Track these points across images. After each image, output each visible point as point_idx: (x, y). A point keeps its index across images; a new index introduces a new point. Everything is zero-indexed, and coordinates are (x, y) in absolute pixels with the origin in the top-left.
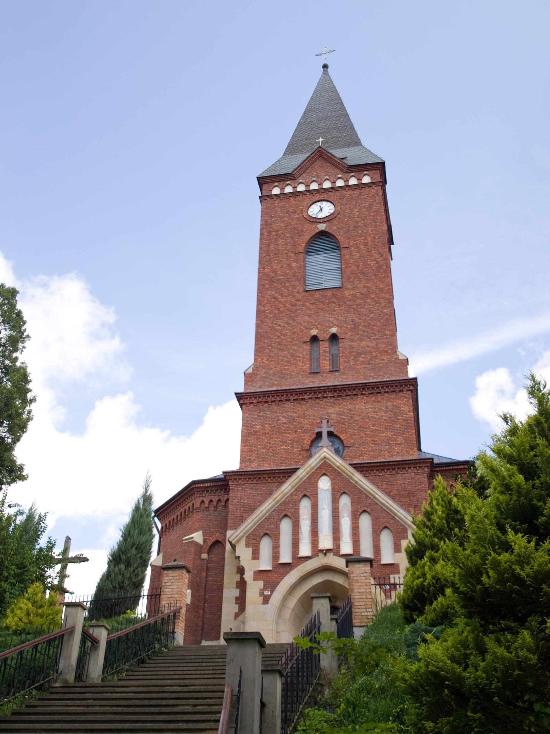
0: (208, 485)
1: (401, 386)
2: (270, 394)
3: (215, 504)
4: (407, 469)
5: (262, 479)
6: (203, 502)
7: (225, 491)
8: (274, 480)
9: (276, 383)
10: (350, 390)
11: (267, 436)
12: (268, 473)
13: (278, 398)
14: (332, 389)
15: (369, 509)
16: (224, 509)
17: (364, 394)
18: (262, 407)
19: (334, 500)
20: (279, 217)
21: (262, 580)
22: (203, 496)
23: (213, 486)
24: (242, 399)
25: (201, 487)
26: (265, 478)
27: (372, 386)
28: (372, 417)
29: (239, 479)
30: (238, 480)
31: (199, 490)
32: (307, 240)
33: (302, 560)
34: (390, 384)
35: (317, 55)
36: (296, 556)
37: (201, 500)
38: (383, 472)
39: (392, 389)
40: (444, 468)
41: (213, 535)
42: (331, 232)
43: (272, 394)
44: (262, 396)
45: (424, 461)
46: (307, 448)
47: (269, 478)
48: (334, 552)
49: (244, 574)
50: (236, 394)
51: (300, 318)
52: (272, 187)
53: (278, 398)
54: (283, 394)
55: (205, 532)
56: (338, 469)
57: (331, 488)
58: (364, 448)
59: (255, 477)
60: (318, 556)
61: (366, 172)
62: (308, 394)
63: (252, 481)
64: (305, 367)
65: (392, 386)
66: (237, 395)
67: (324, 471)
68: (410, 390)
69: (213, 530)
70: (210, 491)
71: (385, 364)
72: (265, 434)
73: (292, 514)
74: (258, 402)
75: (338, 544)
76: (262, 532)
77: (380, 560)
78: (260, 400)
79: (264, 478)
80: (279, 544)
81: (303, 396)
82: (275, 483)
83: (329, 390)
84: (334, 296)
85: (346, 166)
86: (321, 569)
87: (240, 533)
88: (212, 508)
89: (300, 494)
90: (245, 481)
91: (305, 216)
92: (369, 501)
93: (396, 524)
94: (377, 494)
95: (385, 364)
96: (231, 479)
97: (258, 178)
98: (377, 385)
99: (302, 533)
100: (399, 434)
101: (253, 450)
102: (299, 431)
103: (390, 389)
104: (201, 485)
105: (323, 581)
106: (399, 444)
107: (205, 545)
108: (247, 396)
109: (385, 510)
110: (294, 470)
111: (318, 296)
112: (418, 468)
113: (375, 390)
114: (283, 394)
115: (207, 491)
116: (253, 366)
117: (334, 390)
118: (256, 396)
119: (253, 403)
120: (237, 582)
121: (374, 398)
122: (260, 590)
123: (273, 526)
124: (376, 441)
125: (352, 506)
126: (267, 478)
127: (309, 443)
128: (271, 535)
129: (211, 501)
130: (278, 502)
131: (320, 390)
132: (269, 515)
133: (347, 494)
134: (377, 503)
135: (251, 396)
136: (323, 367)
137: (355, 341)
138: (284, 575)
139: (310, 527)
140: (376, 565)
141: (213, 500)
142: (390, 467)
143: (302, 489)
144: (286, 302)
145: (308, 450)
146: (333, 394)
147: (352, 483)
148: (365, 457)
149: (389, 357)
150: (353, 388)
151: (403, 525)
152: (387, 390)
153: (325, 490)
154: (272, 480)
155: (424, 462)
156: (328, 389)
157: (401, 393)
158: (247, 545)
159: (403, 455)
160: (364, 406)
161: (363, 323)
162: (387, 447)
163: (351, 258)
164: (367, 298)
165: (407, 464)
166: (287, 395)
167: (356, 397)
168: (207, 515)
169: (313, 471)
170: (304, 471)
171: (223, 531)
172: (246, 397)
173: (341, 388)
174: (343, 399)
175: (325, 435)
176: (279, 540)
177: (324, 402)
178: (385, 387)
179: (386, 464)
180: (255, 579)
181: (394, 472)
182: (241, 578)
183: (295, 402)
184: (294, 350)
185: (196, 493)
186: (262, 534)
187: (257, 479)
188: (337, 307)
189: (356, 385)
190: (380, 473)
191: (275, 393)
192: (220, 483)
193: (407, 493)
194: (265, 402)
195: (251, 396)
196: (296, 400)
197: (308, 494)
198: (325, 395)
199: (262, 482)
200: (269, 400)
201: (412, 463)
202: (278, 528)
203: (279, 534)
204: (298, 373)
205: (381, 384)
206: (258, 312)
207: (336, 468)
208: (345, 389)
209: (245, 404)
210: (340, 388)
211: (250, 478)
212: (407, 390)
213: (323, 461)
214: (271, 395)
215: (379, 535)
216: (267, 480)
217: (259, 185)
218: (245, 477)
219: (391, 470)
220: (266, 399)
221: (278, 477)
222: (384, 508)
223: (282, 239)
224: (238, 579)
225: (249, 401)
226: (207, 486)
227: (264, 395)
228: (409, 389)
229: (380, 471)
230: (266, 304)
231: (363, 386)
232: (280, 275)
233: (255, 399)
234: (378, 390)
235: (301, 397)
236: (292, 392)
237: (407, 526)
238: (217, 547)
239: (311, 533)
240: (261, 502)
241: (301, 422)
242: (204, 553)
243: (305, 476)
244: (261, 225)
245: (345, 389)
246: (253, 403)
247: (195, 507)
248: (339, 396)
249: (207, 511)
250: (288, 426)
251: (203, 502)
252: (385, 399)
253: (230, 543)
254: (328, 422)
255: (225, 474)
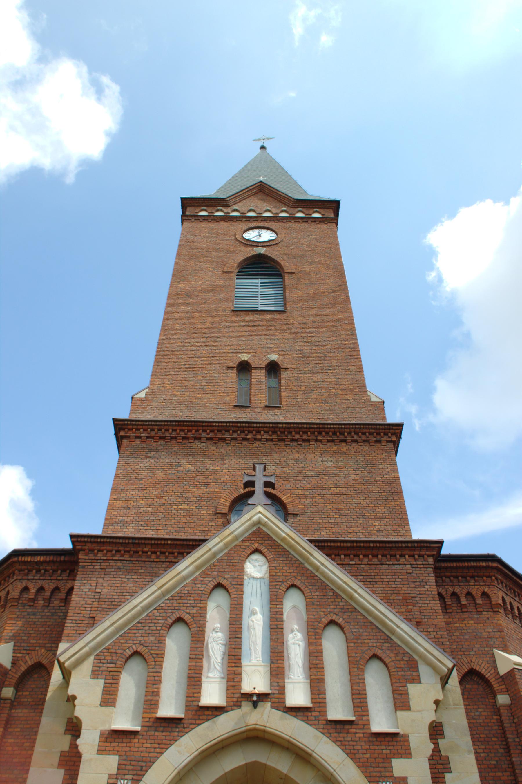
0: (42, 560)
1: (379, 434)
2: (170, 425)
3: (48, 594)
4: (398, 556)
5: (140, 553)
6: (26, 589)
7: (69, 574)
8: (163, 558)
9: (181, 414)
10: (298, 433)
11: (158, 486)
12: (152, 544)
13: (182, 434)
14: (270, 427)
15: (341, 619)
16: (63, 604)
17: (320, 441)
18: (154, 444)
19: (274, 597)
20: (204, 236)
21: (117, 753)
22: (28, 579)
23: (48, 562)
24: (123, 429)
25: (27, 562)
26: (147, 552)
27: (333, 430)
28: (333, 474)
29: (99, 550)
30: (96, 551)
31: (23, 567)
32: (239, 261)
33: (207, 713)
34: (360, 428)
35: (255, 140)
36: (195, 703)
37: (24, 584)
38: (356, 559)
39: (364, 438)
40: (455, 565)
41: (33, 652)
42: (272, 256)
43: (173, 425)
44: (157, 427)
45: (428, 545)
46: (225, 510)
47: (153, 553)
48: (274, 700)
49: (78, 736)
50: (114, 420)
51: (224, 340)
52: (199, 209)
53: (182, 434)
54: (190, 428)
55: (18, 644)
56: (282, 544)
57: (267, 575)
58: (321, 518)
59: (128, 549)
60: (239, 706)
61: (315, 209)
62: (231, 431)
63: (122, 556)
64: (228, 398)
65: (364, 434)
66: (116, 423)
67: (256, 546)
68: (391, 442)
69: (35, 641)
70: (43, 571)
71: (350, 405)
72: (154, 484)
73: (193, 617)
74: (148, 437)
75: (281, 684)
76: (129, 648)
77: (368, 724)
78: (153, 433)
79: (143, 552)
80: (160, 676)
81: (224, 435)
82: (163, 562)
83: (265, 429)
84: (273, 319)
85: (293, 200)
86: (245, 735)
87: (85, 646)
88: (42, 602)
89: (210, 581)
90: (109, 554)
91: (239, 239)
92: (341, 604)
93: (395, 652)
94: (356, 592)
95: (350, 405)
96: (84, 550)
97: (183, 199)
98: (342, 428)
99: (209, 656)
100: (379, 503)
101: (131, 506)
102: (212, 483)
103: (360, 437)
104: (29, 559)
105: (246, 764)
106: (380, 517)
107: (14, 670)
108: (133, 425)
109: (371, 622)
110: (197, 543)
111: (251, 318)
112: (416, 556)
113: (338, 437)
114: (190, 428)
115: (38, 571)
116: (147, 390)
117: (273, 429)
118: (147, 427)
119: (139, 437)
120: (63, 754)
121: (335, 448)
122: (110, 776)
123: (152, 638)
124: (341, 509)
125: (308, 610)
126: (149, 553)
127: (228, 504)
128: (146, 656)
129: (41, 589)
130: (168, 591)
131: (251, 427)
132: (147, 615)
133: (299, 588)
134: (355, 609)
135: (139, 427)
136: (256, 400)
137: (305, 373)
138: (163, 746)
139: (225, 645)
140: (361, 735)
141: (46, 587)
142: (368, 552)
143: (215, 573)
144: (205, 320)
145: (225, 514)
146: (270, 436)
147: (308, 570)
148: (323, 533)
149: (356, 397)
150: (304, 430)
151: (407, 653)
152: (356, 437)
153: (257, 579)
154: (158, 557)
155: (427, 547)
156: (264, 427)
157: (378, 445)
158: (95, 674)
159: (389, 535)
160: (320, 457)
161: (316, 353)
162: (361, 521)
163: (297, 284)
164: (320, 326)
165: (398, 548)
166: (197, 431)
167: (308, 444)
168: (28, 614)
169: (236, 543)
170: (221, 541)
171: (53, 645)
172: (131, 427)
173: (285, 427)
174: (286, 445)
175: (259, 488)
176: (161, 666)
177: (256, 447)
178: (353, 433)
179: (362, 545)
180: (101, 751)
181: (375, 560)
182: (71, 744)
183: (209, 442)
184: (212, 376)
185: (16, 572)
186: (129, 652)
187: (132, 552)
188: (278, 333)
189: (308, 426)
190: (352, 560)
191: (178, 425)
192: (62, 558)
193: (400, 598)
194: (161, 438)
195: (139, 427)
196: (211, 439)
197: (224, 582)
198: (258, 436)
199: (139, 559)
200: (167, 434)
201: (408, 547)
202: (203, 611)
203: (163, 654)
204: (218, 405)
205: (347, 428)
206: (164, 328)
207: (279, 541)
208: (291, 430)
209: (128, 437)
210: (282, 427)
211: (118, 551)
212: (388, 442)
213: (255, 528)
214: (171, 427)
215: (363, 670)
216: (150, 557)
217: (182, 208)
218: (109, 548)
219: (370, 556)
220: (163, 434)
221: (170, 553)
222: (370, 618)
223: (207, 256)
224: (66, 748)
225: (135, 433)
226: (40, 561)
227: (159, 427)
228: (390, 439)
229: (352, 556)
230: (176, 319)
231: (319, 428)
232: (200, 291)
233: (145, 432)
234: (342, 437)
235: (219, 436)
236: (205, 426)
237: (415, 657)
238: (36, 676)
239: (226, 657)
240: (133, 594)
241: (217, 470)
242: (9, 686)
243: (221, 550)
244: (180, 241)
245: (291, 430)
246: (139, 437)
247: (10, 596)
248: (279, 440)
249: (30, 606)
250: (194, 475)
251: (26, 589)
252: (353, 450)
253: (61, 665)
254: (265, 469)
255: (75, 539)
